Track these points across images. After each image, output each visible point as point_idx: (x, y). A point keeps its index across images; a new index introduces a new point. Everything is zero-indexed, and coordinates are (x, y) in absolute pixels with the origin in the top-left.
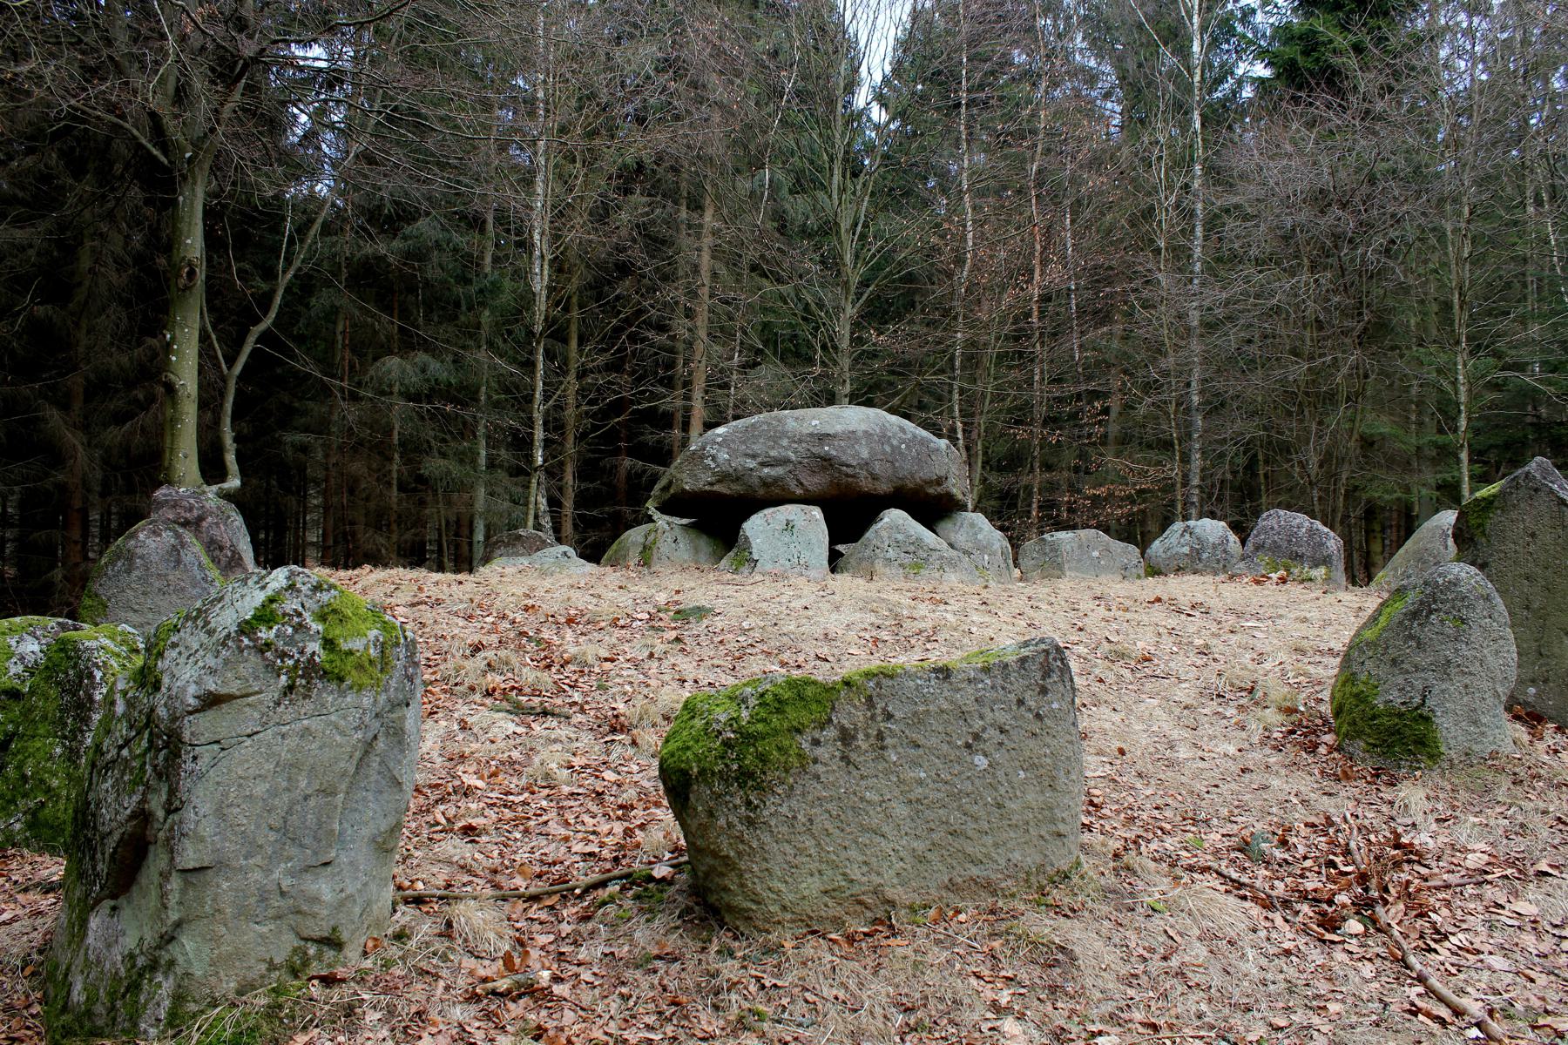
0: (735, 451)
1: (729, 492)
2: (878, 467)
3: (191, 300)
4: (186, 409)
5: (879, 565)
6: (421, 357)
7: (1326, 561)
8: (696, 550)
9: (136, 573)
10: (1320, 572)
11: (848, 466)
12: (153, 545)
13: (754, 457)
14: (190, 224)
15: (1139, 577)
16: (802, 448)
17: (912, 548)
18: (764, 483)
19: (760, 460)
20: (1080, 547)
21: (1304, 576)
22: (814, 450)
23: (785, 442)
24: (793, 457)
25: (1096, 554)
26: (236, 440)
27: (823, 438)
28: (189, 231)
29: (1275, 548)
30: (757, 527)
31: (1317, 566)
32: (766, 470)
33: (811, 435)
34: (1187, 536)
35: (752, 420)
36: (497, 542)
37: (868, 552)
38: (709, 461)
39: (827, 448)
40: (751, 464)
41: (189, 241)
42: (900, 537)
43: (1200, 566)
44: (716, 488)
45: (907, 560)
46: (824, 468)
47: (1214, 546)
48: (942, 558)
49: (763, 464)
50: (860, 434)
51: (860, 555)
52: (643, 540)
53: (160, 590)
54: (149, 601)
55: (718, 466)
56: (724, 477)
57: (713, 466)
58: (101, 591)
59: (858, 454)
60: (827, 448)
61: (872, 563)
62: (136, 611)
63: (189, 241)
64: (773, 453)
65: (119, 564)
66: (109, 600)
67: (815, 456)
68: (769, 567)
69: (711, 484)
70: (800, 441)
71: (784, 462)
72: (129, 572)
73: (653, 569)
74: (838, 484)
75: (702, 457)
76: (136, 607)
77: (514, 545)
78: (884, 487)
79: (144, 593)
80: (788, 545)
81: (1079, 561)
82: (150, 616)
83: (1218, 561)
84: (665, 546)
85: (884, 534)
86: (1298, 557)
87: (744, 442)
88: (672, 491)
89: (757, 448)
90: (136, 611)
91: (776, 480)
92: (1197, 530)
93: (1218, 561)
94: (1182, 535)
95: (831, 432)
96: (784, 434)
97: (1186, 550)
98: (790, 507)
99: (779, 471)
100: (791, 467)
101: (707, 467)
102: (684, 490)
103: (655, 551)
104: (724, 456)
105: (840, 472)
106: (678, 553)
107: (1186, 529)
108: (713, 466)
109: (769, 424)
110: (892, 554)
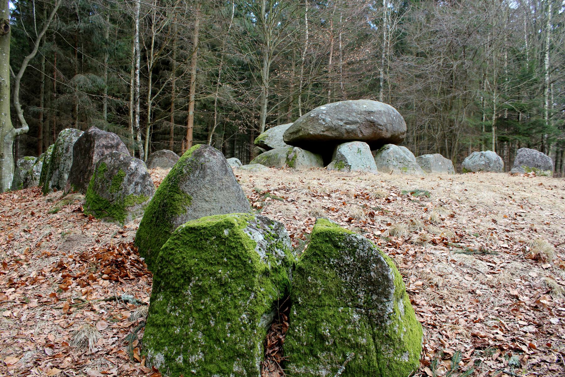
0: (333, 117)
1: (331, 135)
2: (389, 126)
3: (6, 40)
4: (5, 93)
5: (391, 168)
6: (92, 76)
7: (549, 168)
8: (311, 161)
9: (208, 178)
10: (548, 172)
11: (380, 125)
12: (214, 161)
13: (341, 120)
14: (4, 3)
15: (453, 173)
16: (362, 117)
17: (402, 161)
18: (348, 132)
19: (344, 121)
20: (435, 161)
21: (542, 174)
22: (367, 118)
23: (354, 114)
24: (359, 121)
25: (440, 163)
26: (22, 108)
27: (370, 113)
28: (4, 6)
29: (528, 163)
30: (345, 149)
31: (546, 170)
32: (348, 126)
33: (365, 111)
34: (483, 157)
35: (338, 103)
36: (155, 155)
37: (385, 162)
38: (321, 121)
39: (372, 117)
40: (341, 123)
41: (4, 11)
42: (398, 156)
43: (490, 169)
44: (325, 133)
45: (401, 165)
46: (370, 126)
47: (495, 162)
48: (413, 165)
49: (346, 123)
50: (383, 112)
51: (381, 164)
52: (286, 156)
53: (219, 188)
54: (214, 195)
55: (326, 123)
56: (329, 129)
57: (324, 123)
58: (186, 189)
59: (383, 121)
60: (372, 117)
61: (388, 167)
62: (207, 201)
63: (4, 11)
64: (350, 119)
65: (197, 172)
66: (192, 195)
67: (367, 121)
68: (356, 169)
69: (323, 131)
70: (361, 114)
71: (355, 123)
72: (204, 178)
73: (297, 169)
74: (375, 133)
75: (318, 120)
76: (207, 199)
77: (162, 157)
78: (388, 135)
79: (212, 190)
80: (360, 159)
81: (436, 166)
82: (214, 204)
83: (497, 167)
84: (300, 159)
85: (391, 155)
86: (538, 166)
87: (336, 113)
88: (301, 134)
89: (342, 116)
90: (207, 201)
91: (353, 130)
92: (487, 155)
93: (497, 167)
94: (480, 157)
95: (373, 110)
96: (353, 111)
97: (483, 163)
98: (356, 142)
99: (353, 127)
100: (358, 125)
101: (321, 124)
102: (309, 134)
103: (296, 161)
104: (328, 119)
105: (377, 128)
106: (304, 162)
107: (482, 155)
108: (324, 123)
109: (345, 106)
110: (395, 163)
